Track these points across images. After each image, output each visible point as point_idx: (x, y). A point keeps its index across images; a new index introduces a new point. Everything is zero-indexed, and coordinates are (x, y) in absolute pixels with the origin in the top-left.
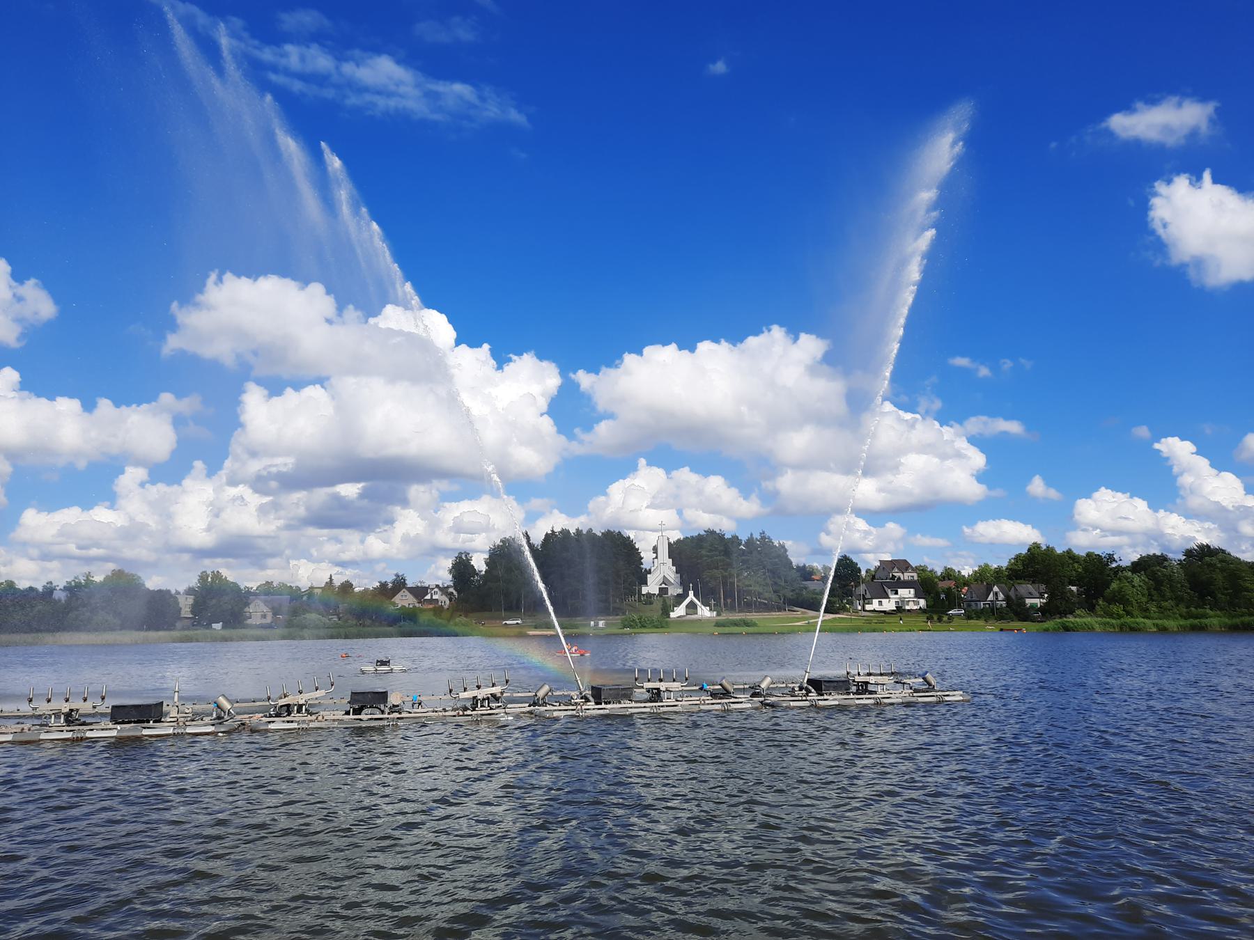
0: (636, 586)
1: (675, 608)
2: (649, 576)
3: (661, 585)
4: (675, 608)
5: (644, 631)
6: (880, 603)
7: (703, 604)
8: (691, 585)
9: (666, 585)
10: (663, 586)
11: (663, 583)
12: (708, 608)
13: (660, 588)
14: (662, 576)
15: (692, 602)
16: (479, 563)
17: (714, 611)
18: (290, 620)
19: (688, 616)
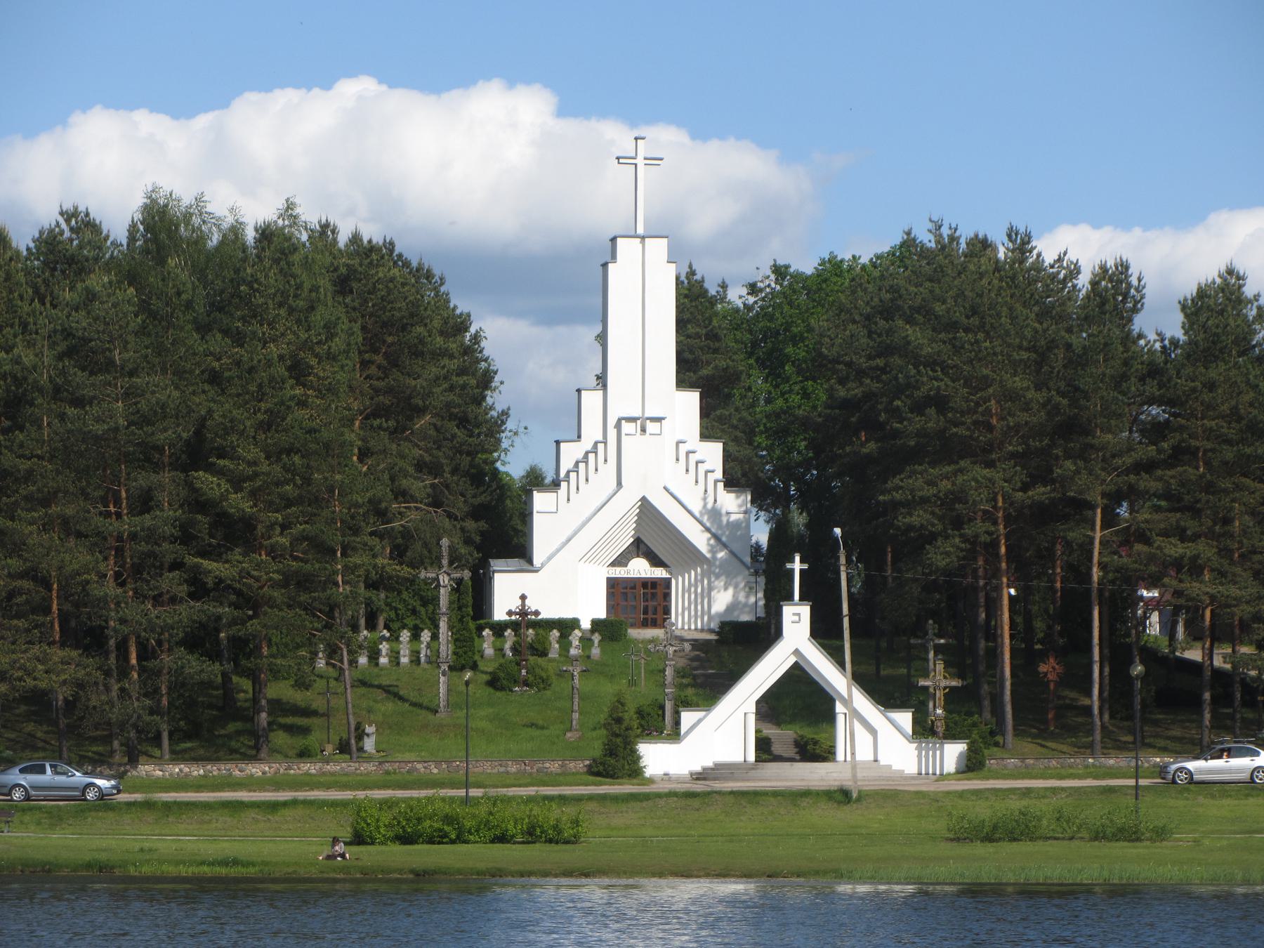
0: (436, 562)
1: (688, 718)
2: (541, 500)
3: (621, 561)
4: (688, 718)
5: (206, 869)
6: (264, 773)
7: (861, 679)
8: (797, 566)
9: (656, 561)
10: (640, 568)
11: (639, 547)
12: (905, 718)
13: (613, 584)
14: (626, 503)
15: (798, 679)
16: (980, 236)
17: (951, 736)
18: (106, 603)
19: (773, 768)
